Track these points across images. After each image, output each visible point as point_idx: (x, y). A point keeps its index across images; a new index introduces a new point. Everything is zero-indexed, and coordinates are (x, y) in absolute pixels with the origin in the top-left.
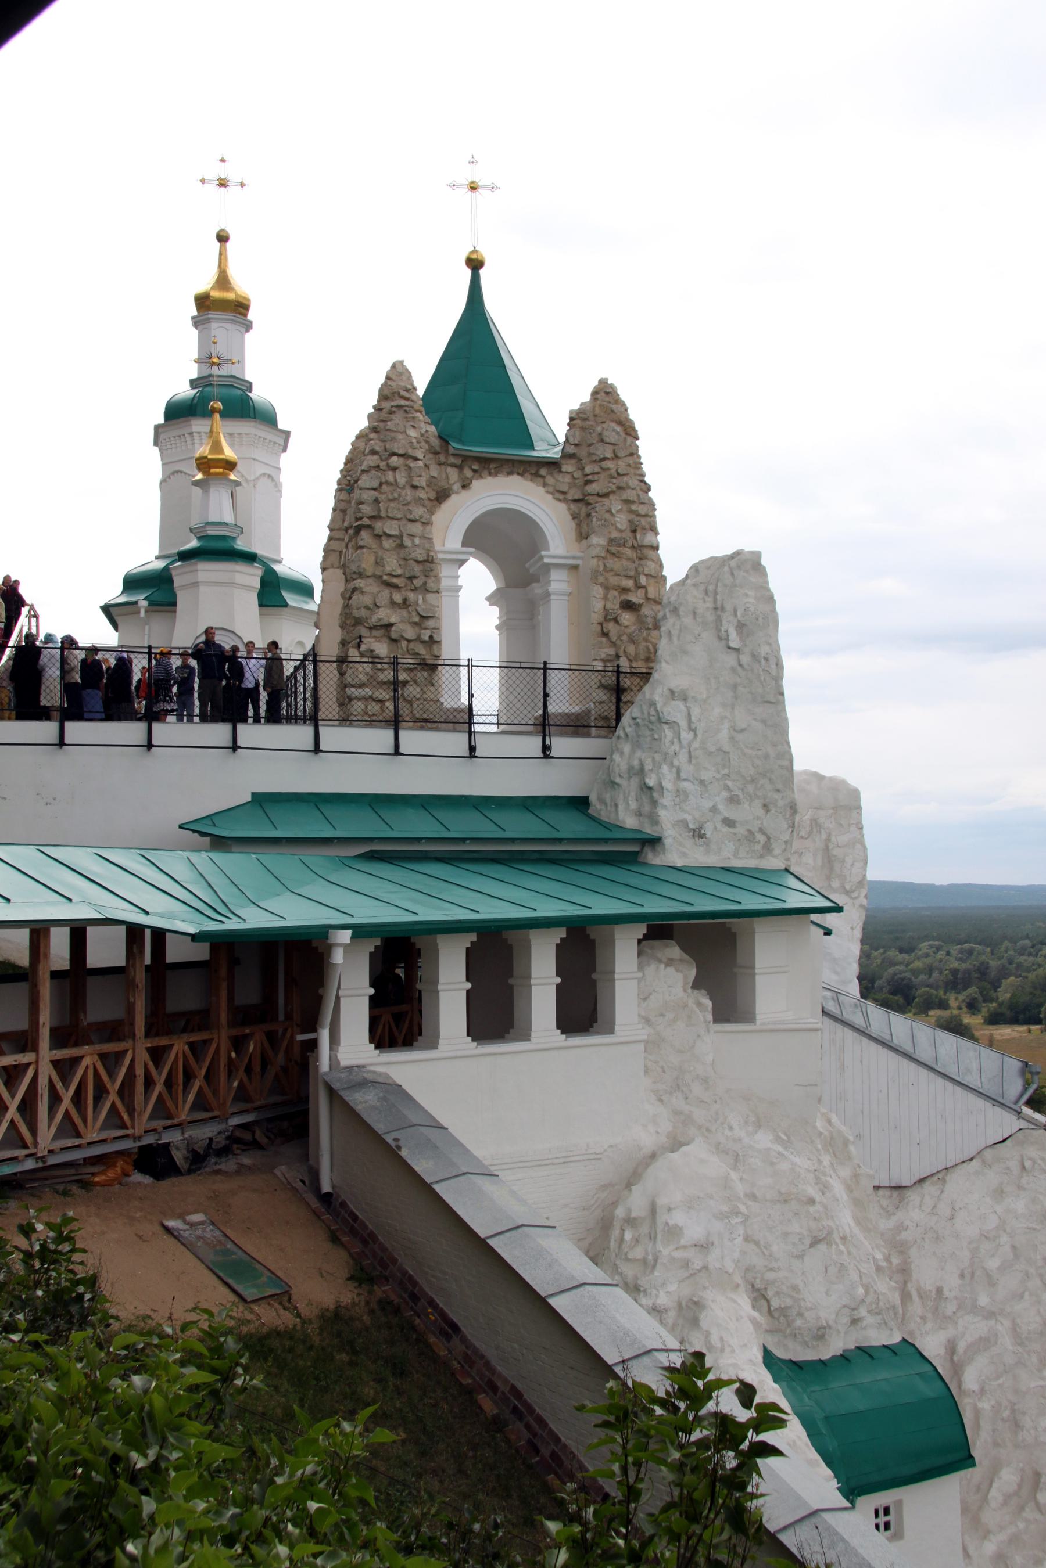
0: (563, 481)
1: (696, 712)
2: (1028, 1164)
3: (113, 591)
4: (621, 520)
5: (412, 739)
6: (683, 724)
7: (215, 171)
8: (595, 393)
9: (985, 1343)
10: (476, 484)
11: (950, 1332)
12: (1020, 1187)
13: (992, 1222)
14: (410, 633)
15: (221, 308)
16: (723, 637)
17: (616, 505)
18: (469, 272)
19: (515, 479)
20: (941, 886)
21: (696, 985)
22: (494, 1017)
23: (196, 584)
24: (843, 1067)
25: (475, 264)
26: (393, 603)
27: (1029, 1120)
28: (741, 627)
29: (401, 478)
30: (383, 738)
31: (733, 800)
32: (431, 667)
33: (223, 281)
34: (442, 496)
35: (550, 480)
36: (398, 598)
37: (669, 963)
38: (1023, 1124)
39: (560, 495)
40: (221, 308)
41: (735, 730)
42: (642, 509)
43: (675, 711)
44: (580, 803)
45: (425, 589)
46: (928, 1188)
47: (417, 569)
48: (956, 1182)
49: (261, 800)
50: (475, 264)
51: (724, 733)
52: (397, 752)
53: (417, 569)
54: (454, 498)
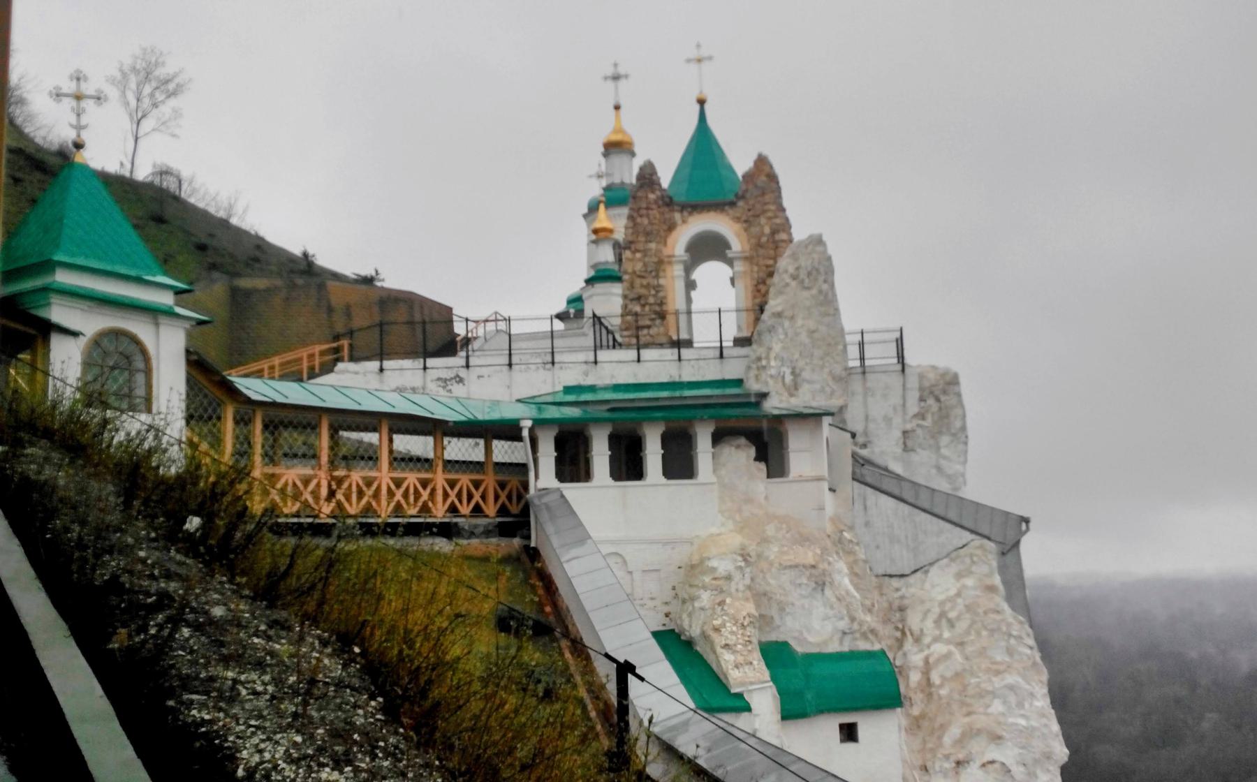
2: (975, 559)
5: (647, 354)
7: (694, 54)
8: (756, 163)
9: (947, 656)
11: (926, 652)
12: (972, 573)
13: (953, 592)
18: (697, 107)
19: (712, 214)
20: (204, 214)
21: (756, 459)
22: (628, 464)
23: (760, 334)
24: (865, 508)
25: (702, 102)
26: (642, 286)
30: (632, 354)
32: (662, 316)
33: (618, 130)
34: (671, 227)
35: (731, 212)
37: (738, 447)
39: (737, 219)
44: (739, 382)
46: (919, 574)
48: (934, 571)
49: (568, 390)
50: (702, 102)
52: (639, 361)
54: (679, 229)
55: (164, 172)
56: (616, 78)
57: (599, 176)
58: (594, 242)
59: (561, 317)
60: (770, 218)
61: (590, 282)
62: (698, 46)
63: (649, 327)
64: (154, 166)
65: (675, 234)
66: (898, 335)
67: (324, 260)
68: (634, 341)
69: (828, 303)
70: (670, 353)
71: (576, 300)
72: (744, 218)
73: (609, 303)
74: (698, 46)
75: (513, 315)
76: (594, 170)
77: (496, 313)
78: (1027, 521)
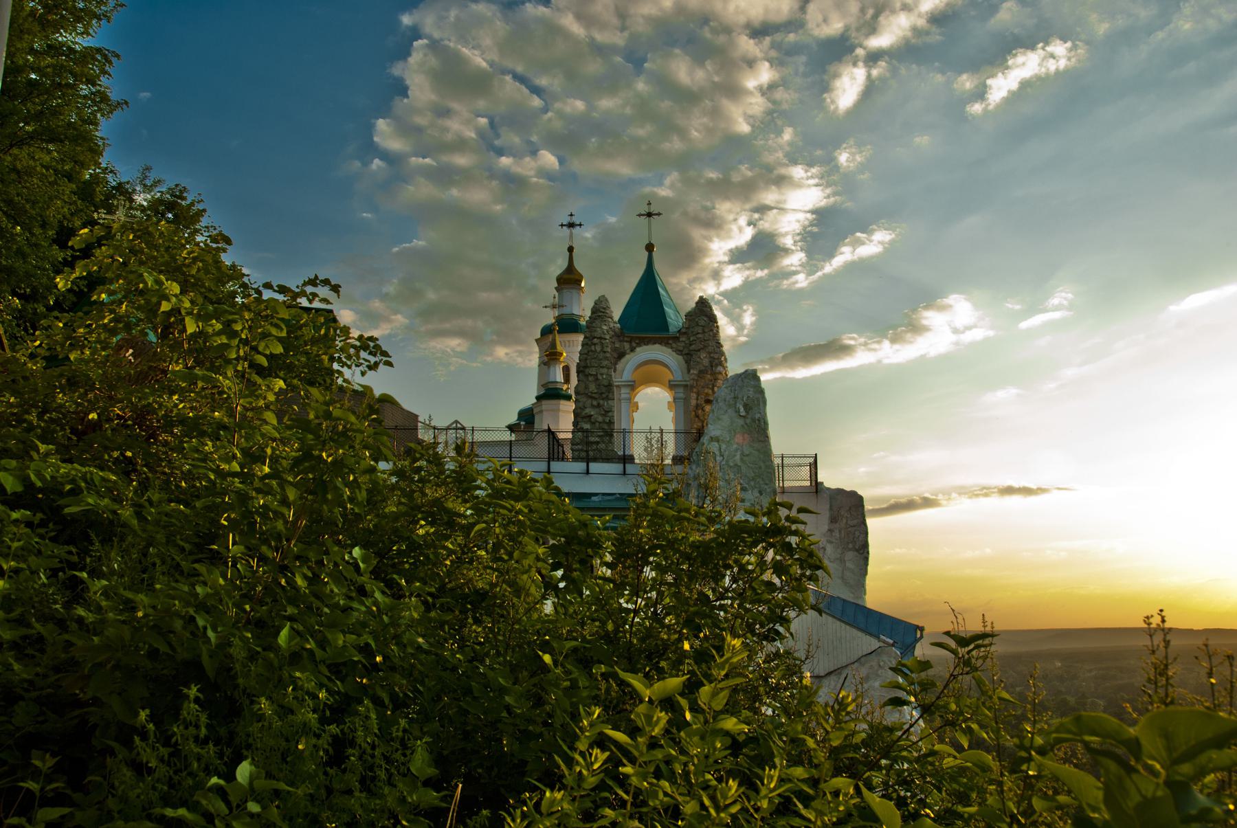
0: (681, 345)
1: (724, 446)
3: (513, 418)
4: (706, 362)
5: (594, 467)
6: (717, 453)
7: (645, 210)
10: (638, 349)
12: (878, 675)
14: (600, 419)
15: (659, 214)
16: (738, 411)
17: (703, 355)
19: (657, 346)
23: (541, 412)
25: (650, 248)
26: (593, 406)
27: (884, 642)
28: (745, 406)
29: (598, 348)
30: (581, 466)
31: (743, 489)
32: (609, 434)
34: (621, 355)
36: (595, 403)
38: (881, 644)
39: (679, 352)
40: (659, 214)
41: (743, 454)
42: (716, 356)
43: (714, 447)
45: (607, 399)
47: (604, 390)
51: (738, 457)
53: (604, 390)
55: (990, 87)
56: (571, 225)
57: (554, 307)
58: (545, 364)
59: (511, 428)
60: (710, 353)
61: (539, 398)
62: (649, 204)
63: (598, 443)
64: (767, 10)
65: (623, 360)
66: (812, 460)
67: (868, 578)
68: (583, 454)
69: (758, 430)
70: (616, 468)
71: (527, 416)
72: (686, 351)
73: (564, 420)
74: (649, 204)
75: (477, 425)
76: (550, 301)
77: (456, 422)
78: (922, 629)
